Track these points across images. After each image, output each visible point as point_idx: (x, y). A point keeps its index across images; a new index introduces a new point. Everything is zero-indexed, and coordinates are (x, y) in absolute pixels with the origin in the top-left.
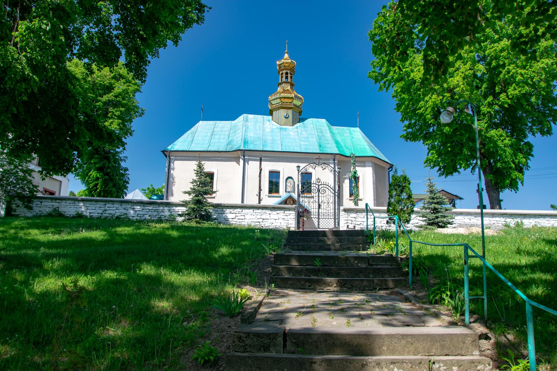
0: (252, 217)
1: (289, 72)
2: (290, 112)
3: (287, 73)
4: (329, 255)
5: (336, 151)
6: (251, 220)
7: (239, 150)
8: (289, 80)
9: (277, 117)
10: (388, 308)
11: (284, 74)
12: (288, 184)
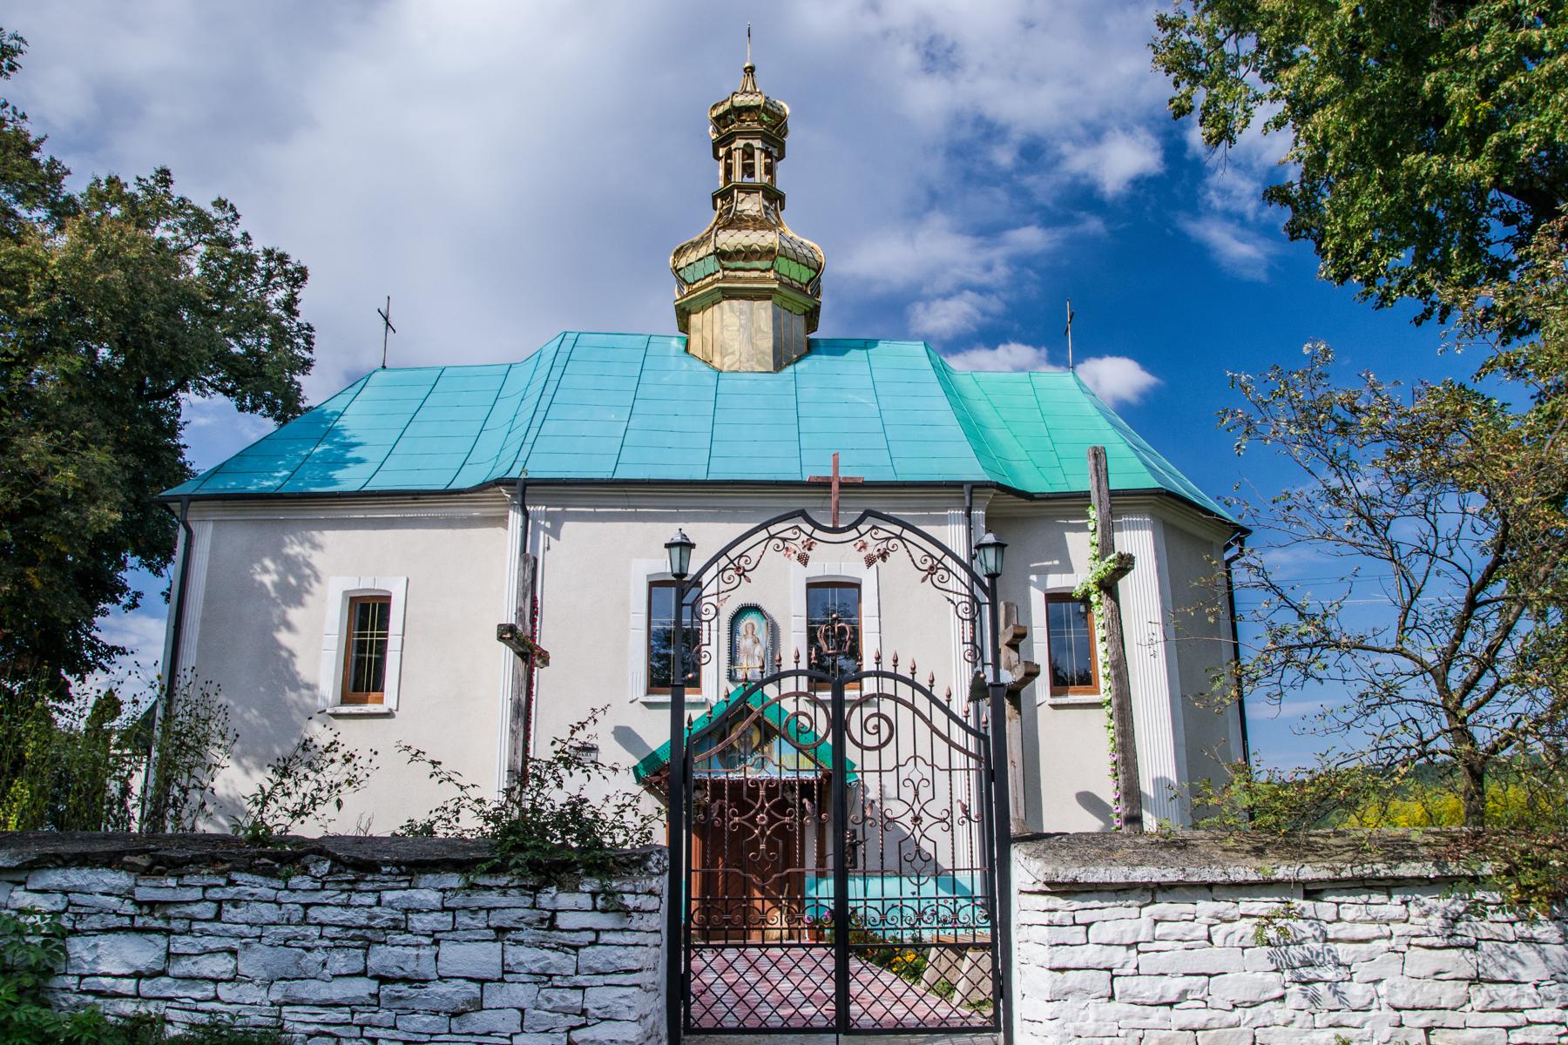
3: (748, 153)
5: (972, 470)
7: (499, 482)
8: (760, 177)
11: (737, 155)
12: (744, 643)
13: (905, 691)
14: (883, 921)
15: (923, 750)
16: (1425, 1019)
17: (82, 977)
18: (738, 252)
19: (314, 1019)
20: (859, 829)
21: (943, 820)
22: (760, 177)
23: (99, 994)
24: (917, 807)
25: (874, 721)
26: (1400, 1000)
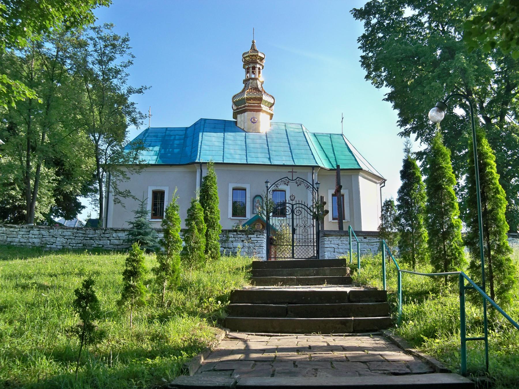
13: (303, 206)
15: (306, 216)
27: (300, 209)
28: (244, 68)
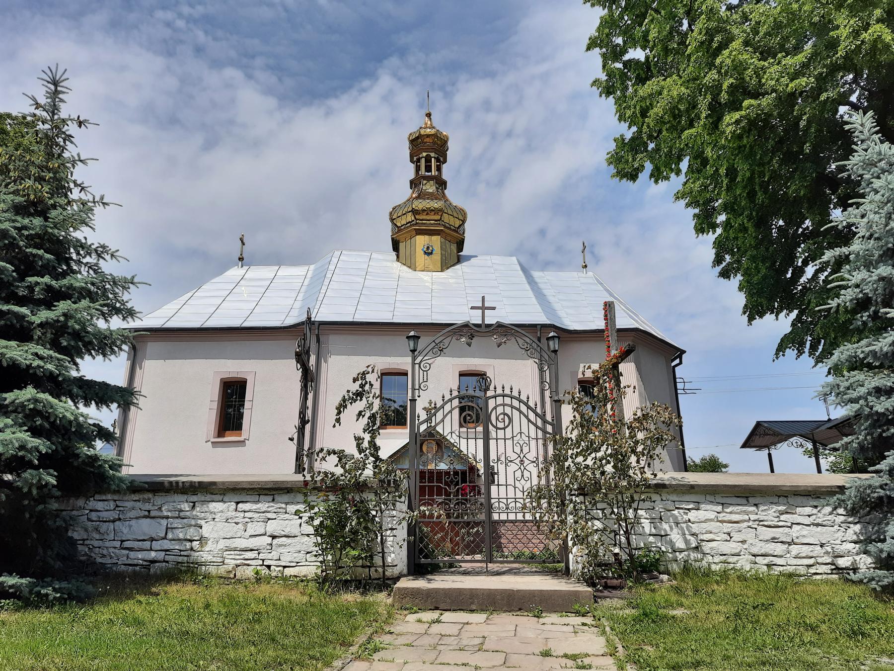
0: (231, 529)
1: (433, 155)
2: (436, 240)
3: (428, 160)
4: (229, 362)
5: (540, 318)
6: (222, 544)
8: (434, 172)
9: (408, 253)
10: (452, 572)
13: (516, 403)
14: (507, 508)
15: (525, 429)
16: (767, 560)
17: (122, 541)
18: (423, 211)
19: (238, 557)
20: (495, 465)
21: (534, 462)
22: (434, 172)
23: (130, 549)
24: (522, 456)
25: (502, 416)
26: (755, 550)
27: (508, 410)
28: (412, 161)
